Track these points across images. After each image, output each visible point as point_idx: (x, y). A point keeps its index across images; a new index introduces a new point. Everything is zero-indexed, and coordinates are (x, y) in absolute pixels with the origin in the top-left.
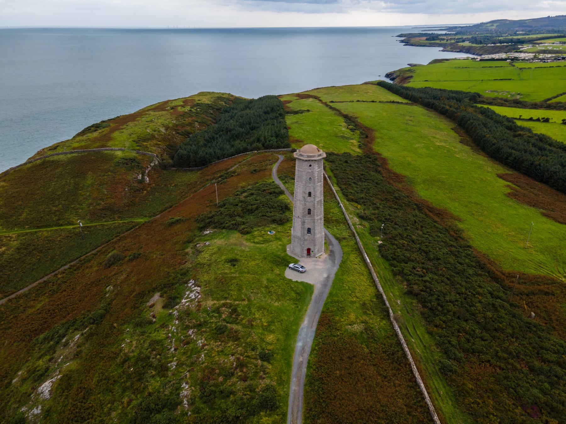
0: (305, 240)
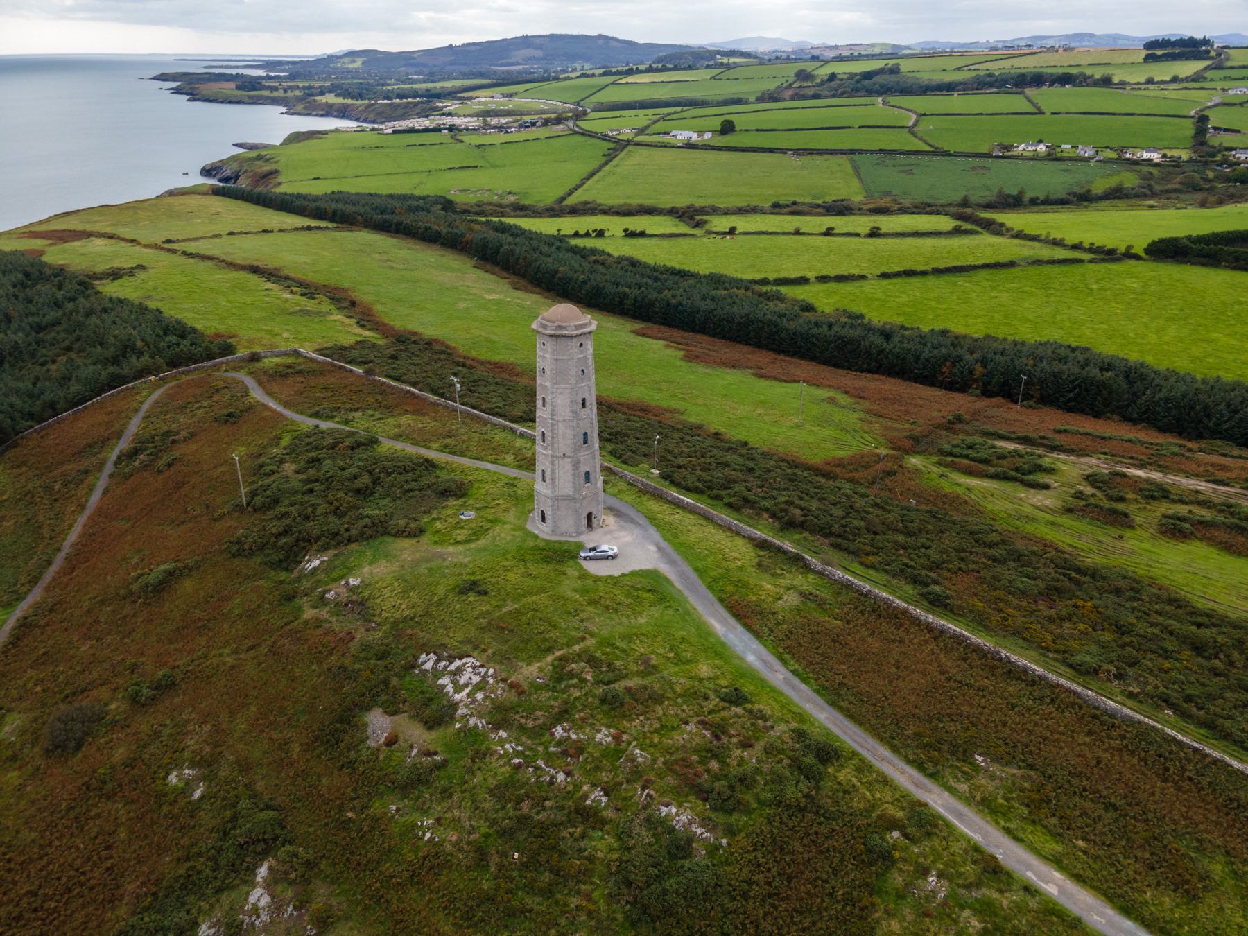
0: (584, 498)
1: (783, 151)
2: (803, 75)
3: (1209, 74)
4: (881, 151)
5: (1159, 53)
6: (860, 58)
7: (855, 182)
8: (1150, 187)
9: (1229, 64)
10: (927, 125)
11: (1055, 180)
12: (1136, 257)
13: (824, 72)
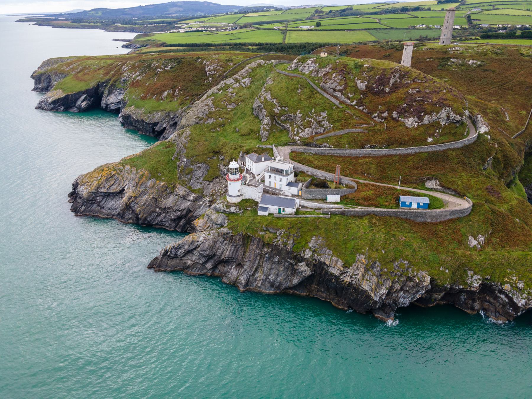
1: (344, 30)
3: (461, 7)
7: (372, 37)
9: (467, 3)
10: (382, 21)
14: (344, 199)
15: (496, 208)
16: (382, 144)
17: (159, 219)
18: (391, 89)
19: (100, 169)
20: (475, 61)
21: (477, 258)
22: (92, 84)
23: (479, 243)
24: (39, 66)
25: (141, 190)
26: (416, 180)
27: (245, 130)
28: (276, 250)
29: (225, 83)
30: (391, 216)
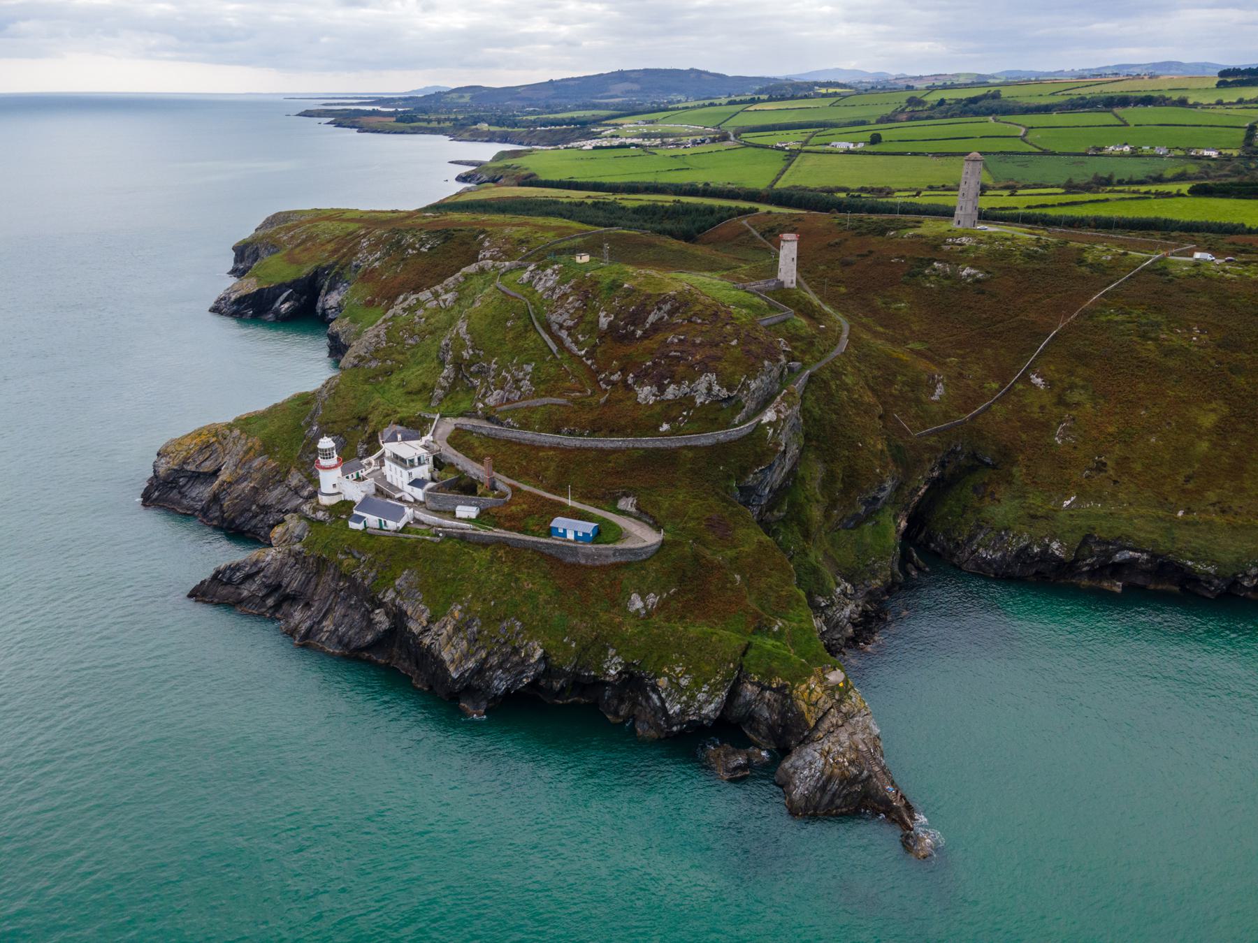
2: (912, 101)
4: (1002, 152)
5: (1230, 80)
6: (953, 87)
8: (1207, 173)
10: (1033, 135)
11: (1137, 169)
12: (1183, 195)
13: (933, 98)
14: (485, 517)
15: (708, 553)
16: (584, 428)
17: (254, 522)
18: (645, 332)
19: (199, 433)
20: (973, 271)
21: (629, 630)
22: (306, 270)
23: (645, 606)
24: (258, 225)
25: (241, 472)
26: (605, 494)
27: (415, 385)
28: (354, 587)
29: (417, 299)
30: (526, 549)
